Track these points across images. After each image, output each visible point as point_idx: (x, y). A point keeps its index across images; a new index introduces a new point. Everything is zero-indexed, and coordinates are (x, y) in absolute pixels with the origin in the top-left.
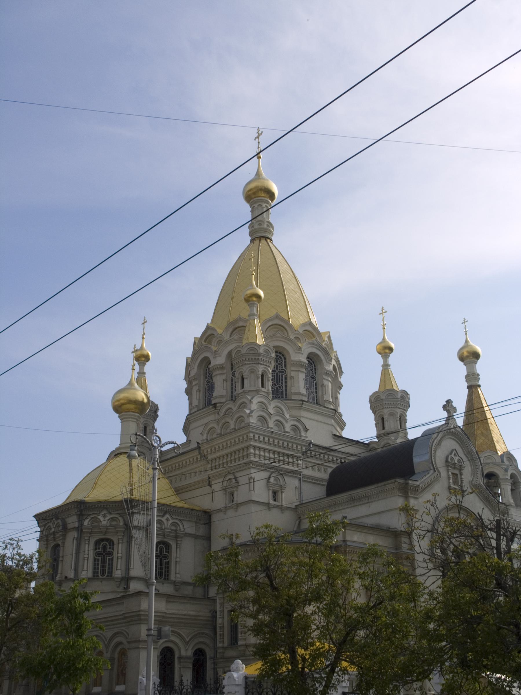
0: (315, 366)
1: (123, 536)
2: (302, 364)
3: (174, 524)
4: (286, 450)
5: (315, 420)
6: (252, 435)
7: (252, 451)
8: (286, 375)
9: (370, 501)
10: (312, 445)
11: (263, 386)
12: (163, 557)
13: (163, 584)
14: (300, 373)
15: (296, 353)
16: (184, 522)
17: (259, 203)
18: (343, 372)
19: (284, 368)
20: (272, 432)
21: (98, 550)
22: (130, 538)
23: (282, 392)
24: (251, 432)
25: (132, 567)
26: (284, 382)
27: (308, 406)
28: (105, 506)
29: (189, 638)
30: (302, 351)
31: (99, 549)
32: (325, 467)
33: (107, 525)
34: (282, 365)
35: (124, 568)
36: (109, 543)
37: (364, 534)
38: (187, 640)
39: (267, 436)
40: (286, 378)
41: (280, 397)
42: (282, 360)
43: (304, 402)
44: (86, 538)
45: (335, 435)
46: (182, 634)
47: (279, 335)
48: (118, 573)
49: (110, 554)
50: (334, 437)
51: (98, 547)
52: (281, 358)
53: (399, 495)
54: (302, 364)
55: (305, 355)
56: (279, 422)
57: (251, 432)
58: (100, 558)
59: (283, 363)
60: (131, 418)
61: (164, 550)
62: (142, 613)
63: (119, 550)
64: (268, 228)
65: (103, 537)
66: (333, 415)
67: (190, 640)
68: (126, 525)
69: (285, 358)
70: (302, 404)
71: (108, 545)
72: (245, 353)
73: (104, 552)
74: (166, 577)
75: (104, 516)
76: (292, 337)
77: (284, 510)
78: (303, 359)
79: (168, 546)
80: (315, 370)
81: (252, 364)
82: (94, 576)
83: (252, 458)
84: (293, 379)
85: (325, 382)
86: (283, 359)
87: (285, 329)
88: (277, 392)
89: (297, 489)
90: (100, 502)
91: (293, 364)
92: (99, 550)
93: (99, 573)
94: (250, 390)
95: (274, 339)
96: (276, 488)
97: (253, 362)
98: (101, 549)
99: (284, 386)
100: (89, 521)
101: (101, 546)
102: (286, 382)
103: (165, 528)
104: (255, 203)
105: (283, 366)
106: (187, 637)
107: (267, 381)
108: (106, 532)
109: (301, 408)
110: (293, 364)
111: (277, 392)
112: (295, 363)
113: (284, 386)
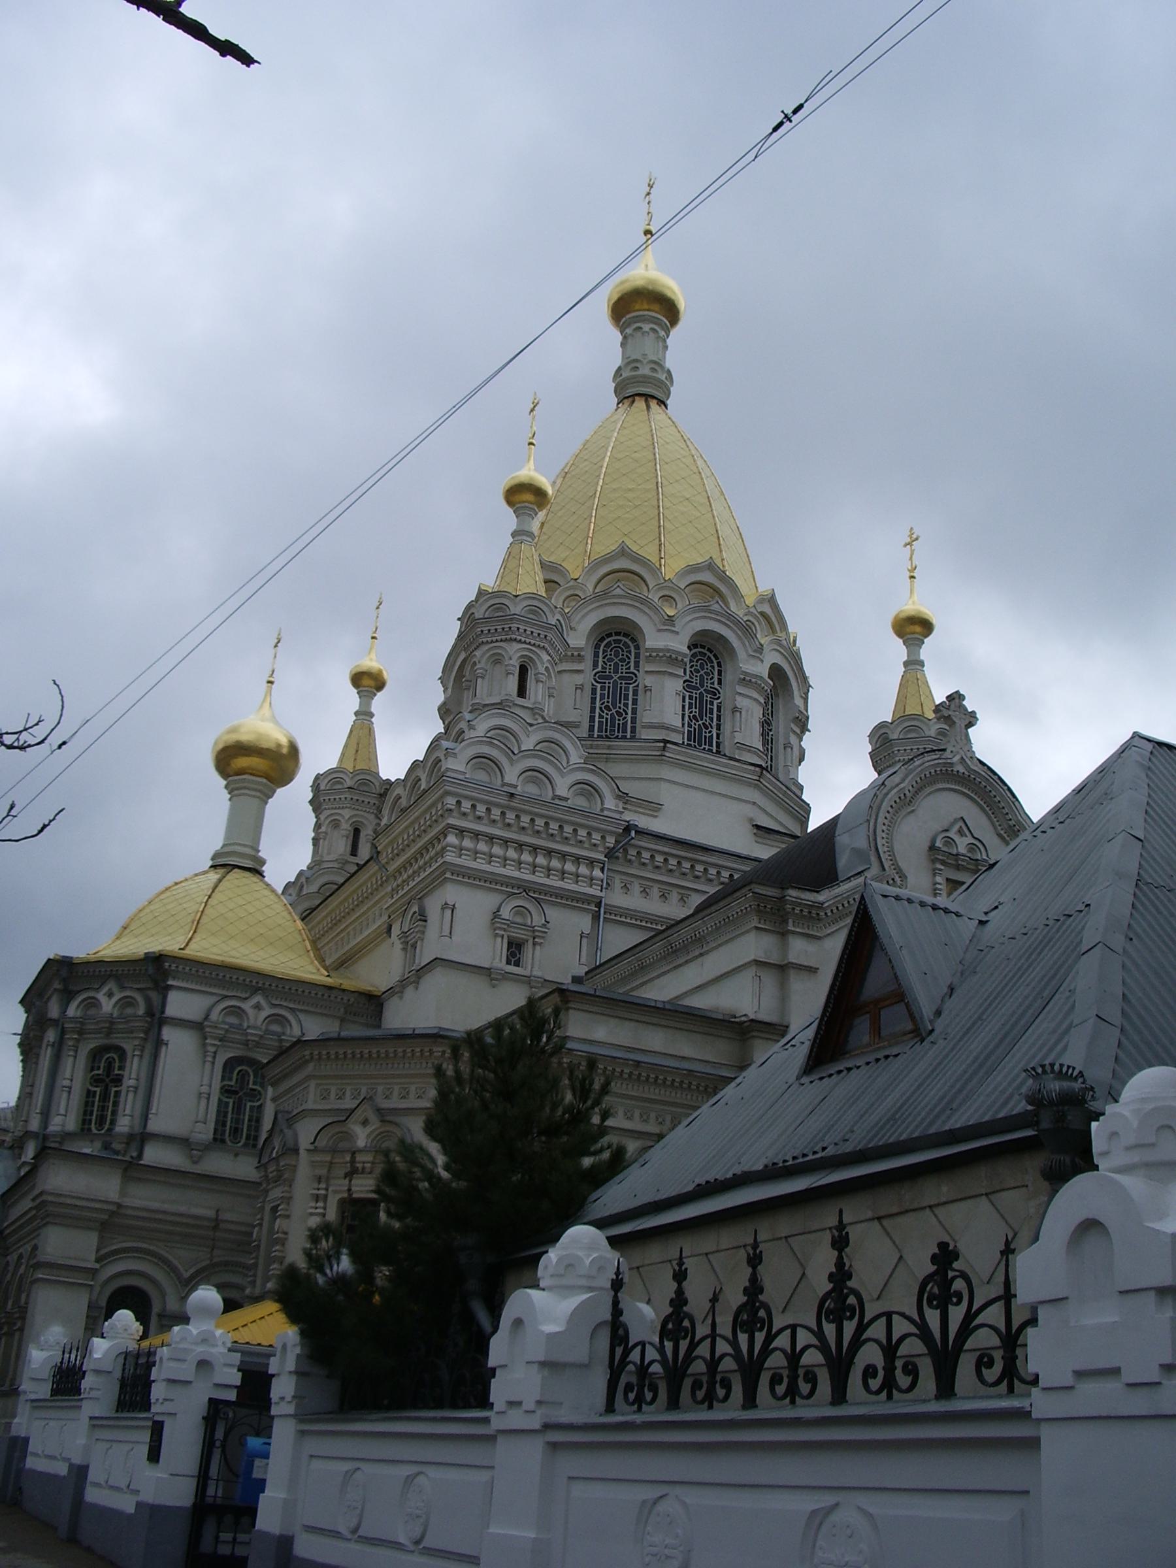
0: (719, 665)
1: (145, 1040)
2: (674, 656)
3: (274, 1018)
4: (557, 842)
5: (703, 790)
6: (451, 801)
7: (452, 839)
8: (594, 670)
9: (705, 949)
10: (636, 832)
11: (522, 692)
12: (236, 1092)
13: (236, 1155)
14: (667, 677)
15: (659, 630)
16: (302, 1016)
17: (638, 325)
18: (810, 686)
19: (716, 686)
20: (512, 795)
21: (96, 1072)
22: (159, 1043)
23: (625, 724)
24: (447, 793)
25: (154, 1111)
26: (630, 702)
27: (679, 753)
28: (114, 973)
29: (192, 1271)
30: (674, 626)
31: (99, 1068)
32: (683, 892)
33: (112, 1014)
34: (604, 658)
35: (138, 1113)
36: (253, 1071)
37: (633, 1024)
38: (187, 1275)
39: (498, 805)
40: (635, 693)
41: (617, 737)
42: (630, 652)
43: (668, 745)
44: (70, 1043)
45: (758, 827)
46: (176, 1262)
47: (618, 591)
48: (124, 1125)
49: (227, 1091)
50: (755, 831)
51: (96, 1065)
52: (619, 641)
53: (757, 928)
54: (674, 656)
55: (767, 665)
56: (530, 770)
57: (447, 793)
58: (231, 1101)
59: (632, 658)
60: (248, 789)
61: (117, 1065)
62: (50, 1198)
63: (133, 1071)
64: (655, 375)
65: (106, 1042)
66: (758, 778)
67: (192, 1277)
68: (150, 1013)
69: (637, 647)
70: (664, 748)
71: (117, 1061)
72: (481, 617)
73: (236, 1092)
74: (251, 1142)
75: (258, 1007)
76: (655, 597)
77: (497, 980)
78: (763, 670)
79: (122, 1053)
80: (720, 673)
81: (497, 641)
82: (82, 1130)
83: (450, 857)
84: (649, 693)
85: (741, 702)
86: (630, 643)
87: (645, 581)
88: (613, 725)
89: (585, 941)
90: (100, 962)
91: (650, 656)
92: (229, 1083)
93: (93, 1122)
94: (487, 702)
95: (608, 601)
96: (519, 934)
97: (499, 638)
98: (234, 1080)
99: (630, 712)
100: (78, 1006)
101: (102, 1065)
102: (635, 702)
103: (249, 1027)
104: (629, 325)
105: (632, 664)
106: (186, 1271)
107: (534, 682)
108: (109, 1033)
109: (660, 759)
110: (650, 656)
111: (613, 725)
112: (654, 654)
113: (630, 712)
